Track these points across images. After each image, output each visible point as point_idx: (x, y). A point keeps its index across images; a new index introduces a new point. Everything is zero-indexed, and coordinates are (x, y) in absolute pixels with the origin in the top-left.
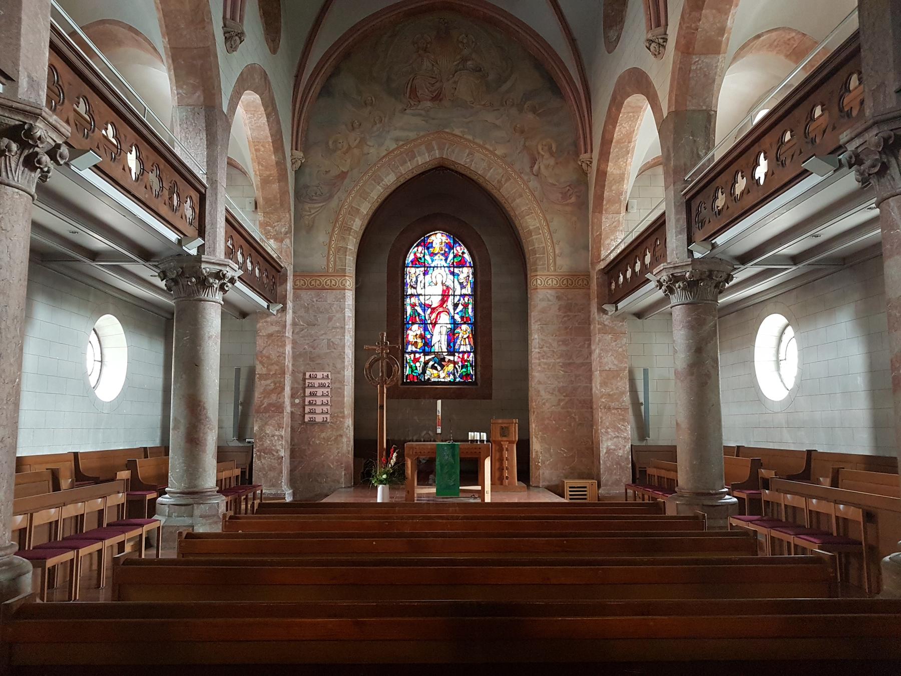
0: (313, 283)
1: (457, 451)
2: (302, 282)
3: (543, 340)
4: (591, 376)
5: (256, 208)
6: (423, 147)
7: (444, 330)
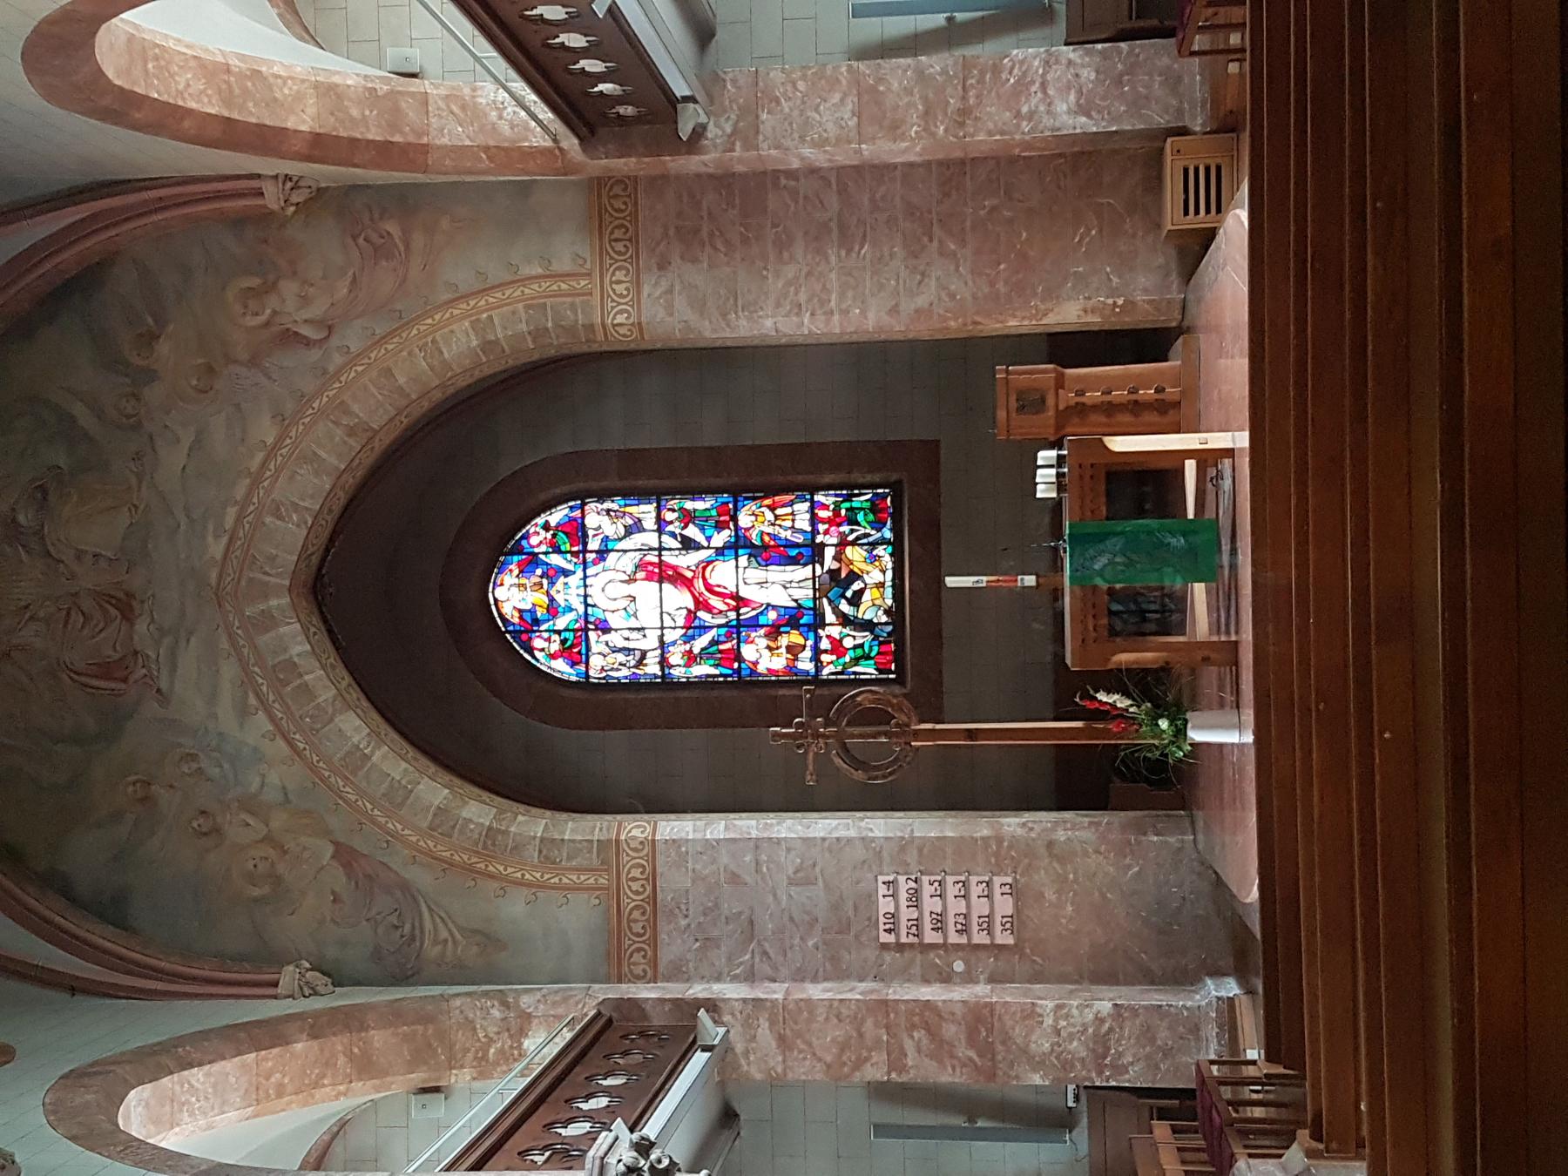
0: (637, 928)
1: (1091, 527)
2: (637, 957)
3: (778, 305)
4: (874, 166)
5: (437, 1090)
6: (264, 640)
7: (755, 574)
